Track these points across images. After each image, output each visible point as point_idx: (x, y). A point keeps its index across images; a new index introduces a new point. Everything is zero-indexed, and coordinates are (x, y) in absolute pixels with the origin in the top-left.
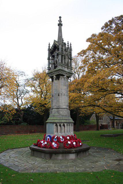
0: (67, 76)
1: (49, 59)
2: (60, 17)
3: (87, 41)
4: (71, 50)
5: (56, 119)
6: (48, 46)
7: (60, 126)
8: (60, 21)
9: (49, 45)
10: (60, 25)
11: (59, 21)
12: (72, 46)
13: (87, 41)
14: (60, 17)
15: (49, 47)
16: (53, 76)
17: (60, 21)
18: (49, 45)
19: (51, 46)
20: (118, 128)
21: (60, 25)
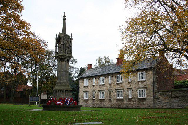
0: (67, 59)
1: (71, 46)
2: (64, 13)
3: (59, 33)
4: (72, 39)
5: (60, 88)
6: (56, 36)
7: (67, 92)
8: (64, 16)
9: (56, 35)
10: (64, 19)
11: (63, 16)
12: (72, 38)
13: (59, 33)
14: (64, 13)
15: (56, 37)
16: (65, 59)
17: (64, 16)
18: (56, 35)
19: (57, 36)
20: (86, 98)
21: (64, 19)
